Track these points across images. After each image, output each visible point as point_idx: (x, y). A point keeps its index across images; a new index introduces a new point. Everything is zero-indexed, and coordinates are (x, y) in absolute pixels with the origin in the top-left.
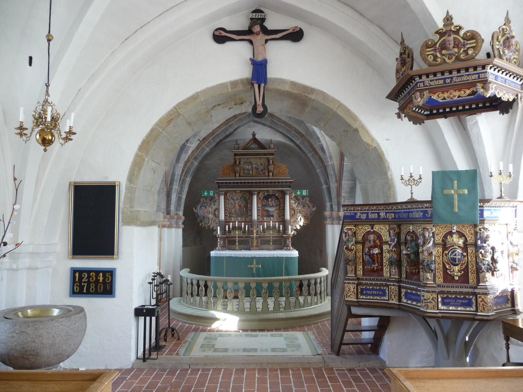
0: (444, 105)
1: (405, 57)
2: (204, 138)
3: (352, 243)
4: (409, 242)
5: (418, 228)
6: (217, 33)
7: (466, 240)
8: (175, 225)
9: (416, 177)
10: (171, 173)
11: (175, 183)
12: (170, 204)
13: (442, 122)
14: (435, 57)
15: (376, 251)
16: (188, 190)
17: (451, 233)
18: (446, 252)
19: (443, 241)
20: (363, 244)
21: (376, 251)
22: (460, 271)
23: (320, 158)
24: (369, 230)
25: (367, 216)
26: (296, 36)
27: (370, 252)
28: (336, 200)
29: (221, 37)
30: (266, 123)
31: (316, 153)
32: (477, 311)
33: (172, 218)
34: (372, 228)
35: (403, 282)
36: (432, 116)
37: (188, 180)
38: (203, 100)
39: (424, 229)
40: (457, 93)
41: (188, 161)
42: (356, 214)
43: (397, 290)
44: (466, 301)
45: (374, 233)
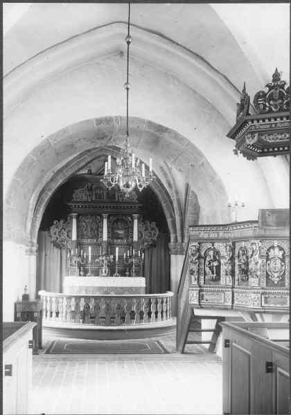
0: (273, 146)
1: (243, 106)
4: (241, 255)
7: (284, 253)
9: (240, 205)
13: (270, 160)
14: (265, 106)
15: (215, 264)
17: (273, 247)
19: (267, 253)
21: (215, 264)
34: (213, 245)
36: (263, 154)
39: (252, 244)
40: (280, 137)
44: (283, 300)
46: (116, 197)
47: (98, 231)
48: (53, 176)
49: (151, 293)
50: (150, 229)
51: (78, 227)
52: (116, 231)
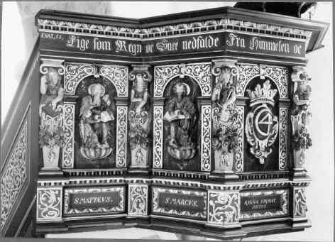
3: (59, 99)
5: (198, 70)
18: (251, 115)
20: (78, 103)
21: (106, 117)
22: (267, 149)
24: (90, 74)
25: (91, 45)
27: (93, 119)
32: (126, 211)
34: (98, 71)
35: (156, 175)
43: (146, 191)
45: (101, 81)
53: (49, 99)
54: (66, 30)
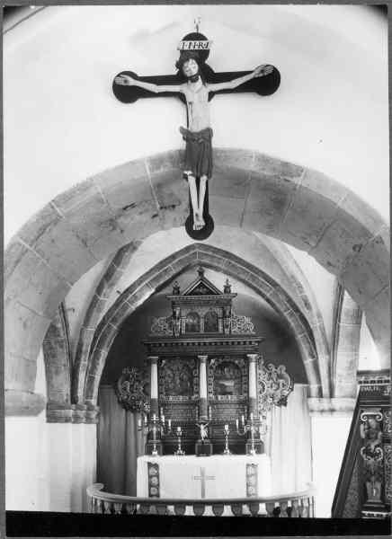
2: (127, 290)
3: (376, 443)
6: (121, 82)
8: (84, 420)
10: (77, 342)
11: (83, 357)
12: (77, 388)
16: (105, 367)
23: (303, 318)
26: (266, 83)
28: (327, 381)
29: (127, 92)
30: (220, 266)
31: (297, 310)
33: (80, 408)
37: (104, 353)
38: (100, 190)
41: (102, 324)
42: (383, 388)
46: (220, 328)
47: (192, 383)
48: (118, 299)
49: (124, 494)
50: (274, 376)
51: (159, 377)
52: (221, 382)
53: (369, 442)
54: (381, 382)
